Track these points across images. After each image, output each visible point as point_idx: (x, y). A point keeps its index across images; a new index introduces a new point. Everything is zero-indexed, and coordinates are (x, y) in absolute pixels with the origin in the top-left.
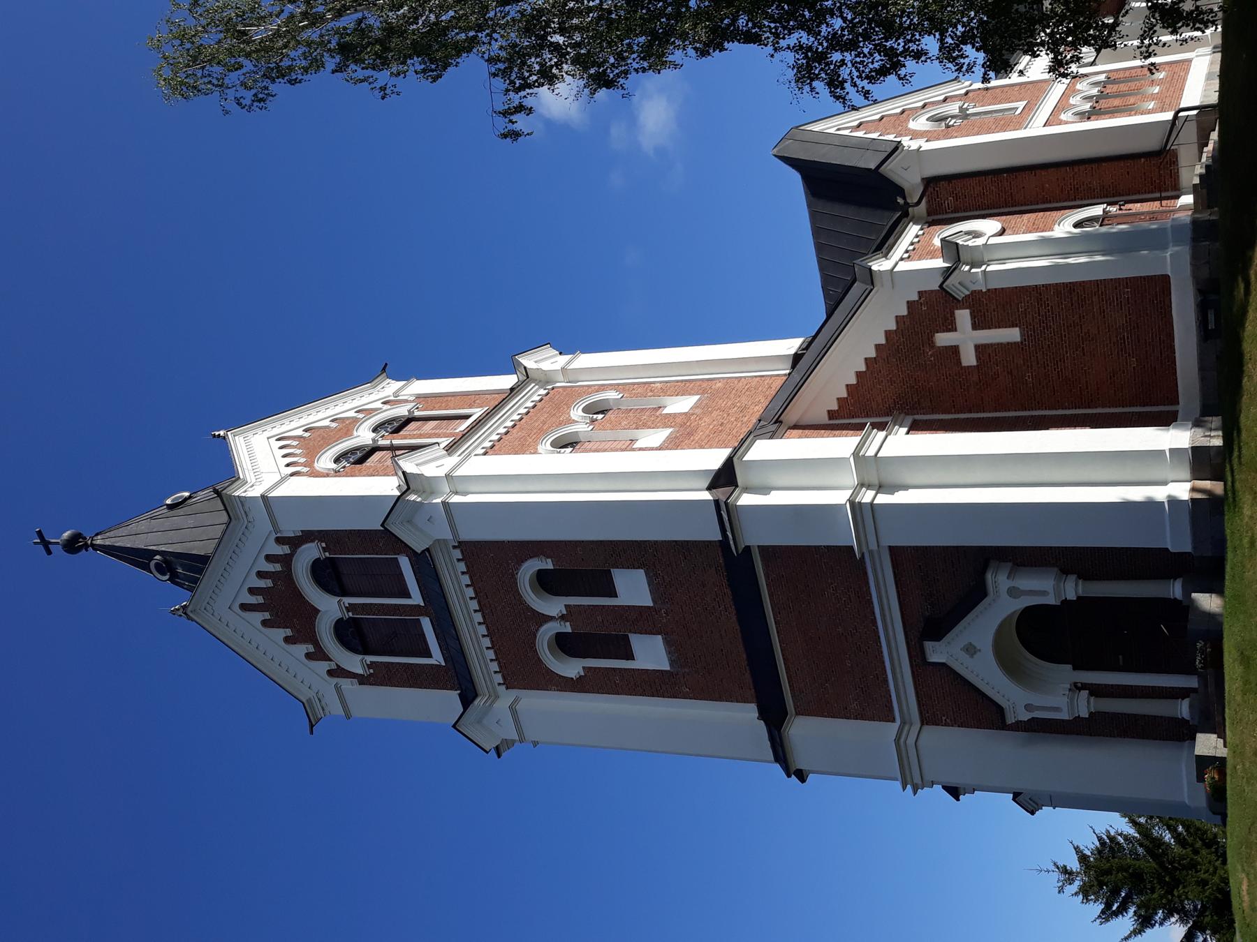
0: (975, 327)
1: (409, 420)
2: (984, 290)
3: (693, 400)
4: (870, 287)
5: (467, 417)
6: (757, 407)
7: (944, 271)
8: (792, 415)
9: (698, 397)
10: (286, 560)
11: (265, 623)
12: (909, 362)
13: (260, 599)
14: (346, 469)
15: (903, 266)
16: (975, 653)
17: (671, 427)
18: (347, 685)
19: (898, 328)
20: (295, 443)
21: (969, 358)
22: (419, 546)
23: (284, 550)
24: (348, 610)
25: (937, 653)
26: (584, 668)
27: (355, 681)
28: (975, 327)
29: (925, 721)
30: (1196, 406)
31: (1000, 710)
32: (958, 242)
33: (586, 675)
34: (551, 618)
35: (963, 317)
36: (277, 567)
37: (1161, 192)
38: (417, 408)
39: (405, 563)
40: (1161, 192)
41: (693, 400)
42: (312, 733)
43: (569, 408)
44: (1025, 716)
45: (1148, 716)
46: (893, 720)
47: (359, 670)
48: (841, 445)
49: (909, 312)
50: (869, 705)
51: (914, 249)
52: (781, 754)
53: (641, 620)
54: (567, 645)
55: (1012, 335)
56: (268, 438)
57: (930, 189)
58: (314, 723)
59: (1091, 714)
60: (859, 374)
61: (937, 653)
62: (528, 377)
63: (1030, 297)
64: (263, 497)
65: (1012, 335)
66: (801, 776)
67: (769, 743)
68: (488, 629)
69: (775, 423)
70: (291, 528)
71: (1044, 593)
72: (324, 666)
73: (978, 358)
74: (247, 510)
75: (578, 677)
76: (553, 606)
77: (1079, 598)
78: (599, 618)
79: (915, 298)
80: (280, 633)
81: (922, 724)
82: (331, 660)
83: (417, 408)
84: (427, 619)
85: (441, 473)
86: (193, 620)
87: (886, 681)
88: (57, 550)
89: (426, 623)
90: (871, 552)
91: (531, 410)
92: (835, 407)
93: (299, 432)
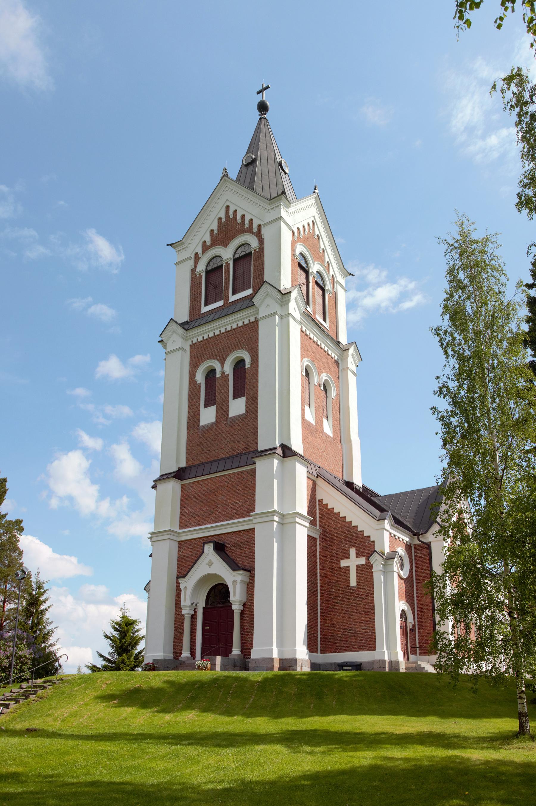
0: (358, 566)
1: (323, 290)
2: (373, 570)
3: (330, 434)
4: (377, 519)
5: (324, 320)
6: (326, 465)
7: (383, 552)
8: (320, 482)
9: (332, 436)
10: (250, 230)
11: (220, 219)
13: (231, 216)
14: (296, 260)
15: (386, 534)
16: (209, 565)
17: (316, 424)
18: (192, 262)
19: (358, 532)
20: (311, 231)
21: (344, 563)
22: (255, 300)
23: (255, 230)
24: (227, 263)
26: (200, 383)
27: (193, 267)
28: (358, 566)
29: (180, 542)
30: (314, 661)
31: (185, 576)
32: (396, 559)
33: (197, 384)
34: (223, 367)
35: (362, 561)
36: (247, 225)
37: (419, 647)
38: (330, 294)
39: (249, 292)
40: (419, 647)
41: (330, 434)
42: (168, 245)
43: (328, 372)
44: (182, 587)
46: (180, 529)
47: (198, 269)
48: (302, 507)
49: (365, 537)
51: (396, 539)
52: (163, 478)
53: (222, 412)
54: (211, 374)
55: (353, 582)
56: (314, 216)
57: (426, 546)
58: (173, 246)
59: (183, 615)
60: (338, 513)
61: (209, 549)
62: (344, 350)
64: (280, 218)
65: (353, 582)
66: (154, 487)
68: (218, 335)
69: (318, 475)
70: (266, 233)
71: (234, 595)
72: (199, 250)
73: (344, 567)
74: (275, 209)
76: (228, 369)
77: (233, 611)
78: (223, 391)
79: (372, 540)
80: (215, 227)
81: (179, 542)
82: (203, 254)
83: (330, 294)
84: (222, 304)
85: (291, 311)
86: (221, 180)
87: (197, 525)
88: (259, 98)
89: (220, 303)
90: (252, 520)
91: (326, 353)
92: (324, 503)
93: (317, 232)
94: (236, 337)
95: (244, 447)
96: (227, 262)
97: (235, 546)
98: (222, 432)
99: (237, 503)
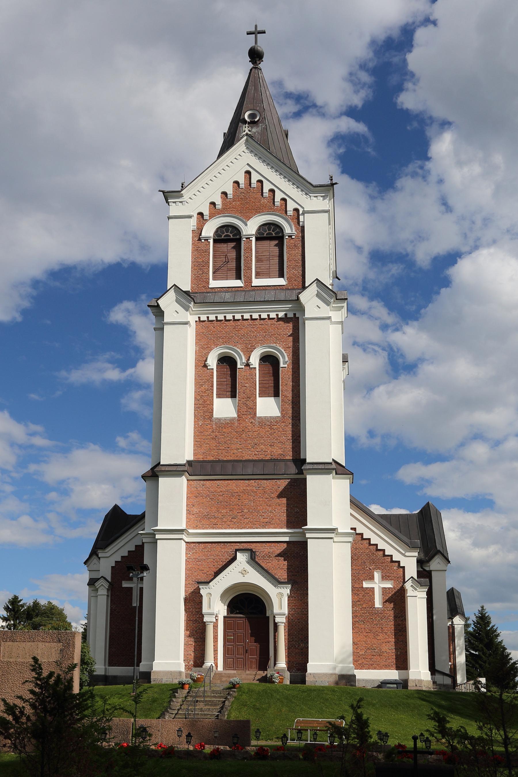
12: (367, 558)
18: (193, 222)
25: (241, 557)
45: (205, 647)
50: (196, 517)
59: (205, 622)
63: (398, 613)
67: (173, 463)
75: (207, 365)
94: (266, 329)
95: (279, 453)
96: (249, 238)
97: (269, 557)
98: (248, 430)
99: (271, 512)
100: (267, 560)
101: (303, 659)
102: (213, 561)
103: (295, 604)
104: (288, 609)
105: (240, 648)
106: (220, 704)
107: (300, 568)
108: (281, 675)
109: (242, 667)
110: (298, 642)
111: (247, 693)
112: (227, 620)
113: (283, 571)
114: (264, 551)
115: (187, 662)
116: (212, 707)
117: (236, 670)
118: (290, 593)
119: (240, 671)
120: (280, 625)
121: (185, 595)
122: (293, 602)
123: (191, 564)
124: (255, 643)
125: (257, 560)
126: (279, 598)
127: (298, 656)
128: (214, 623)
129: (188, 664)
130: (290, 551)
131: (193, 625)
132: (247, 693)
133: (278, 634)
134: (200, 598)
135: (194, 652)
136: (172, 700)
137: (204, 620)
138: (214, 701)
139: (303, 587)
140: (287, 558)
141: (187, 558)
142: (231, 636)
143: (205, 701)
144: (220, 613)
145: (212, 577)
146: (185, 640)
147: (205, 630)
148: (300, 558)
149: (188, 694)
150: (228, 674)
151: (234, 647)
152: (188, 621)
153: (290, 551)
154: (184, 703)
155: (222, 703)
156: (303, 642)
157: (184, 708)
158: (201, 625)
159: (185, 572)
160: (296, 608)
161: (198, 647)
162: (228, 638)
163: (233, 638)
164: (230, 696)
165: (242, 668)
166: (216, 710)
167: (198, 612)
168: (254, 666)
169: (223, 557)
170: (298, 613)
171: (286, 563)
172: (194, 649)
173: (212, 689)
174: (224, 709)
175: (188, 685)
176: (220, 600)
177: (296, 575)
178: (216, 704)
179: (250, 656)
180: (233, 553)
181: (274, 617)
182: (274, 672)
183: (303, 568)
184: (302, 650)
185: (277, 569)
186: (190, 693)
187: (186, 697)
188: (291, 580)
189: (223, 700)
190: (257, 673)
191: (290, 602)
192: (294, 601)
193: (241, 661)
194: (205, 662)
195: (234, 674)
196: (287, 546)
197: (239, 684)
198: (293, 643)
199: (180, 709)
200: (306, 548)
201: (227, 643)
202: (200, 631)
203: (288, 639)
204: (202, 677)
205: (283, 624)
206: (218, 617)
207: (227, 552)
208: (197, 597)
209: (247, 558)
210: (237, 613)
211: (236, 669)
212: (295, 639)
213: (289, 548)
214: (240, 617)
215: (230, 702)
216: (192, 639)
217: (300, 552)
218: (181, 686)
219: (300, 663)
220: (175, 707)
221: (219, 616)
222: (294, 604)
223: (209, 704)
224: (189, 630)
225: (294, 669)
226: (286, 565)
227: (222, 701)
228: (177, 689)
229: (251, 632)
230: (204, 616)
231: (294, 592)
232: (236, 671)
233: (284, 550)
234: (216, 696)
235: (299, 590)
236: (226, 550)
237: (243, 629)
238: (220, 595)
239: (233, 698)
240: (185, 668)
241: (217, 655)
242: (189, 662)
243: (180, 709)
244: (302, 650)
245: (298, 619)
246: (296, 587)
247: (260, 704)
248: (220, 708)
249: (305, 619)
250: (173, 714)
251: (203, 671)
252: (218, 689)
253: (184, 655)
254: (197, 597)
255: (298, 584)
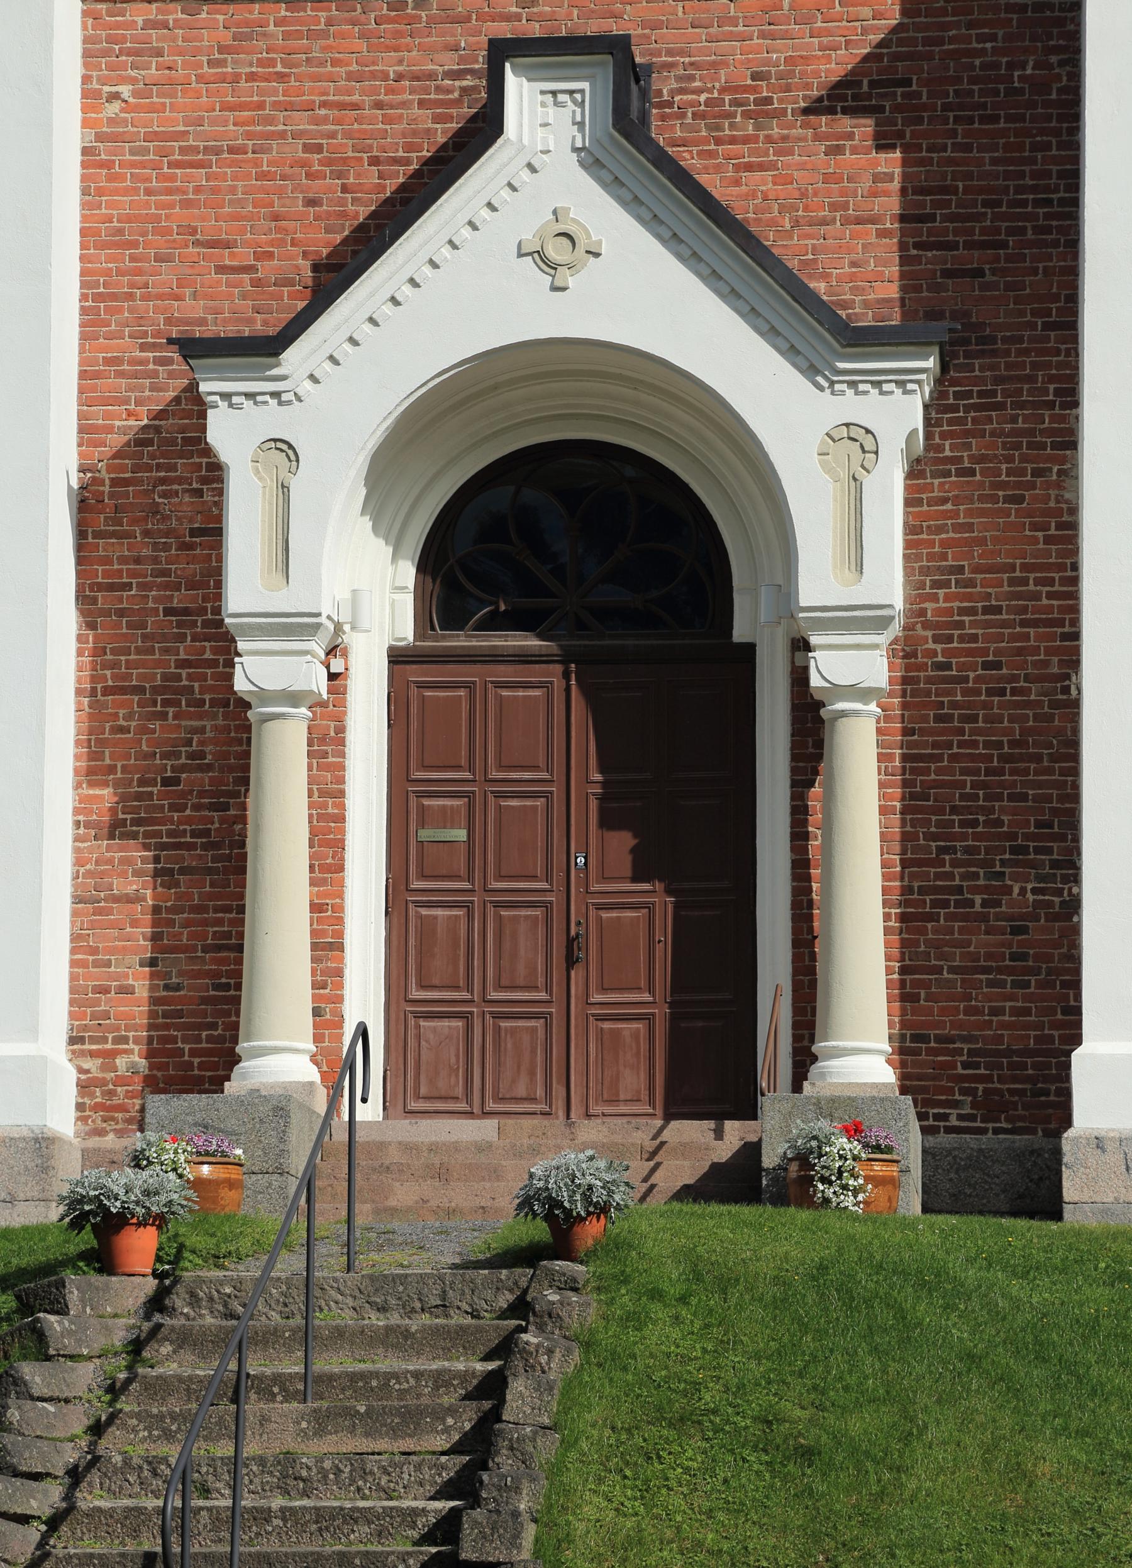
97: (763, 111)
100: (746, 140)
101: (1027, 1012)
102: (304, 164)
103: (970, 527)
104: (908, 571)
105: (523, 927)
106: (451, 1411)
107: (1013, 204)
108: (877, 1148)
109: (540, 1092)
110: (987, 864)
111: (683, 1299)
112: (422, 686)
113: (873, 239)
114: (714, 65)
115: (93, 1054)
116: (382, 1444)
117: (486, 1114)
118: (928, 436)
119: (527, 1123)
120: (843, 714)
121: (82, 470)
122: (945, 515)
123: (126, 192)
124: (635, 879)
125: (659, 134)
126: (844, 475)
127: (991, 984)
128: (318, 704)
129: (103, 1068)
130: (929, 56)
131: (143, 730)
132: (683, 1299)
133: (829, 798)
134: (199, 493)
135: (153, 962)
136: (18, 1382)
137: (240, 684)
138: (395, 1376)
139: (1031, 379)
140: (907, 122)
141: (91, 134)
142: (446, 819)
143: (321, 1379)
144: (364, 624)
145: (301, 305)
146: (79, 862)
147: (246, 768)
148: (1009, 119)
149: (157, 1318)
150: (433, 1148)
151: (470, 916)
152: (107, 691)
153: (929, 56)
154: (125, 1405)
155: (467, 1397)
156: (1032, 865)
157: (127, 1462)
158: (208, 724)
159: (82, 258)
160: (977, 569)
161: (187, 924)
162: (426, 834)
163: (461, 834)
164: (541, 1328)
165: (533, 1100)
166: (427, 1473)
167: (186, 612)
168: (633, 1080)
169: (387, 120)
170: (987, 610)
171: (891, 162)
172: (155, 938)
173: (370, 1261)
174: (505, 1461)
175: (151, 1231)
176: (363, 513)
177: (980, 273)
178: (421, 1412)
179: (604, 990)
180: (468, 82)
181: (801, 646)
182: (823, 1125)
183: (1037, 203)
184: (1023, 930)
185: (824, 222)
186: (171, 1311)
187: (136, 1347)
188: (934, 315)
189: (480, 1367)
190: (666, 1135)
191: (927, 517)
192: (957, 500)
193: (526, 1039)
194: (242, 1047)
195: (482, 1148)
196: (904, 12)
197: (603, 1210)
198: (950, 876)
199: (91, 1464)
200: (1060, 22)
201: (416, 885)
202: (206, 777)
203: (905, 837)
204: (233, 1173)
205: (873, 707)
206: (345, 654)
207: (417, 78)
208: (179, 480)
209: (581, 125)
210: (492, 623)
211: (491, 1106)
212: (964, 837)
213: (918, 28)
214: (524, 658)
215: (551, 1389)
216: (138, 855)
217: (1011, 66)
218: (87, 1239)
219: (1009, 1053)
220: (44, 1445)
221: (353, 640)
222: (957, 528)
223: (354, 1414)
224: (112, 769)
225: (956, 1104)
226: (896, 185)
227: (464, 1376)
228: (49, 1269)
229: (605, 784)
230: (241, 646)
231: (961, 421)
232: (491, 1124)
233: (881, 44)
234: (407, 1334)
235: (1000, 406)
236: (415, 60)
237: (549, 755)
238: (360, 462)
239: (569, 1351)
240: (80, 1107)
241: (341, 986)
242: (113, 1054)
243: (91, 1464)
244: (1016, 931)
245: (986, 666)
246: (977, 381)
247: (821, 1408)
248: (454, 1450)
249: (1046, 664)
250: (23, 1519)
251: (232, 1124)
252: (419, 1264)
253: (72, 990)
254: (179, 480)
255: (994, 353)
